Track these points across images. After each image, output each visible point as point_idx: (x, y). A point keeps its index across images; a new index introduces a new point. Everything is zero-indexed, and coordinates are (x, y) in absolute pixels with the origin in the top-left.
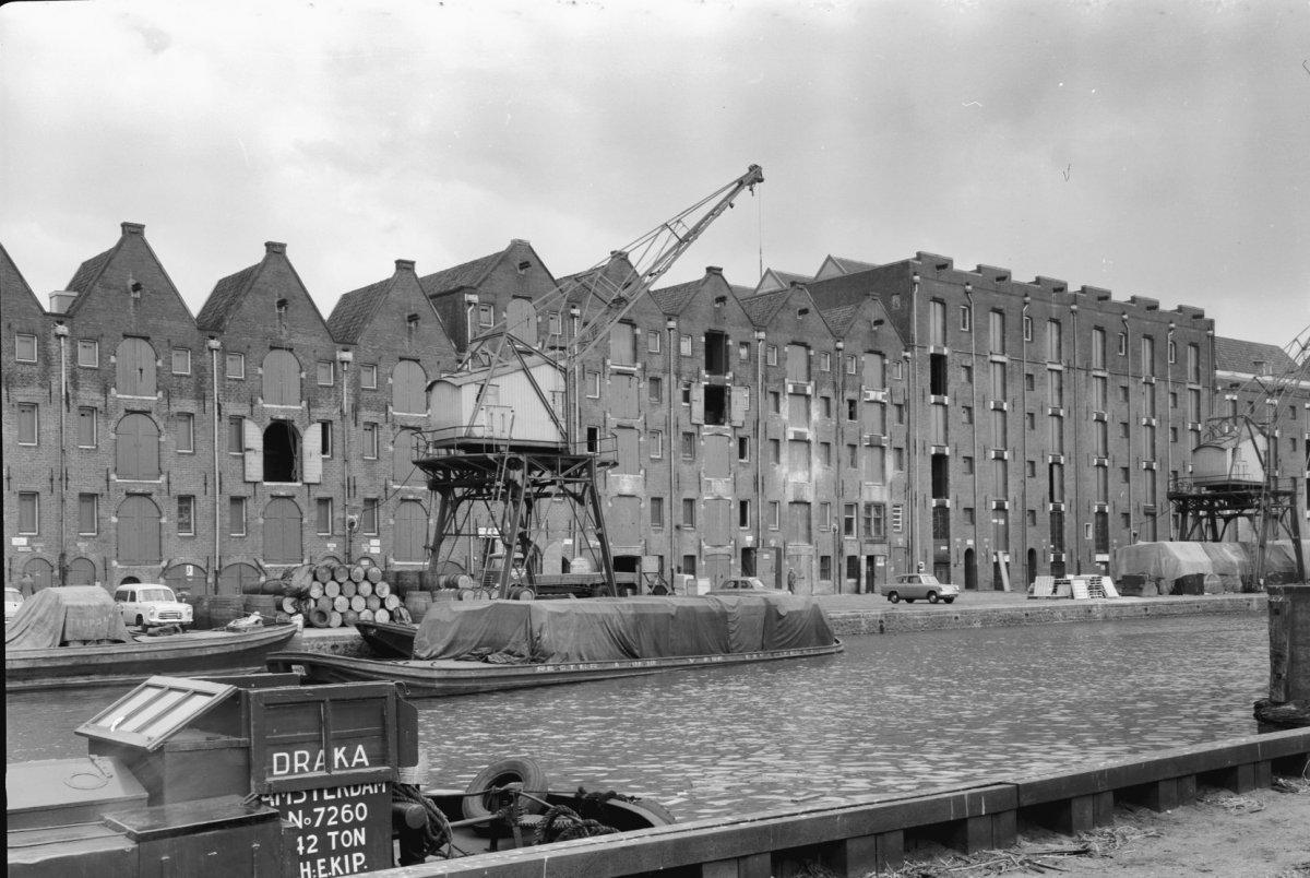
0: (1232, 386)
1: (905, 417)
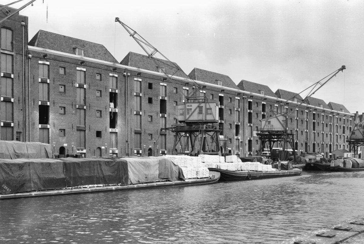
0: (222, 91)
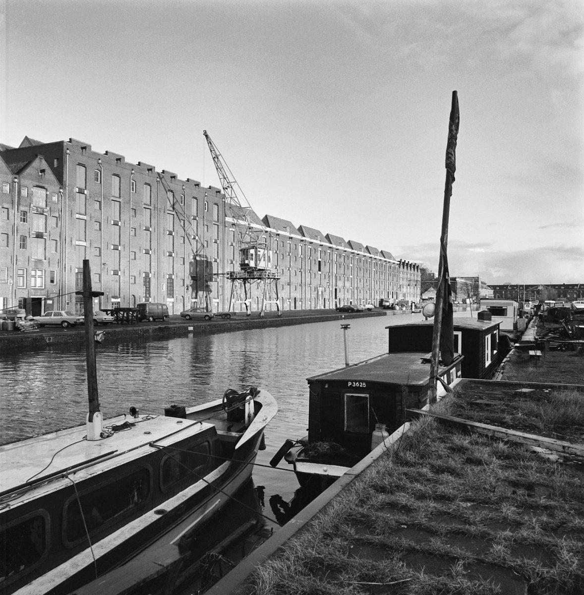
1: (59, 224)
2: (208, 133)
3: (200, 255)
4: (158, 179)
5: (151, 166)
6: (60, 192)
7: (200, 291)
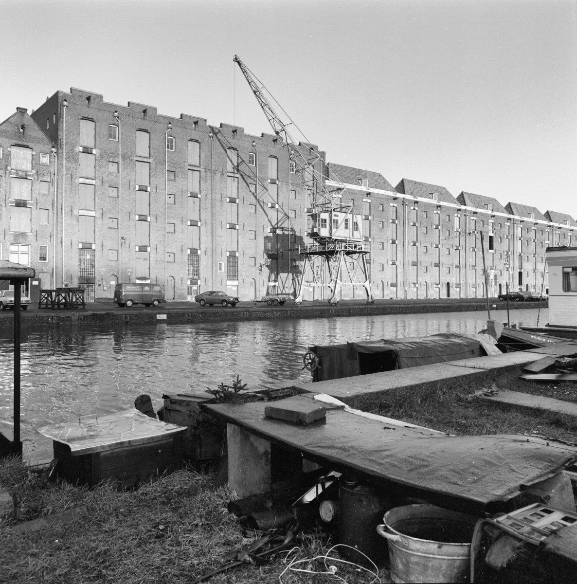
2: (241, 59)
3: (283, 228)
4: (211, 134)
5: (197, 118)
6: (52, 152)
7: (283, 272)
